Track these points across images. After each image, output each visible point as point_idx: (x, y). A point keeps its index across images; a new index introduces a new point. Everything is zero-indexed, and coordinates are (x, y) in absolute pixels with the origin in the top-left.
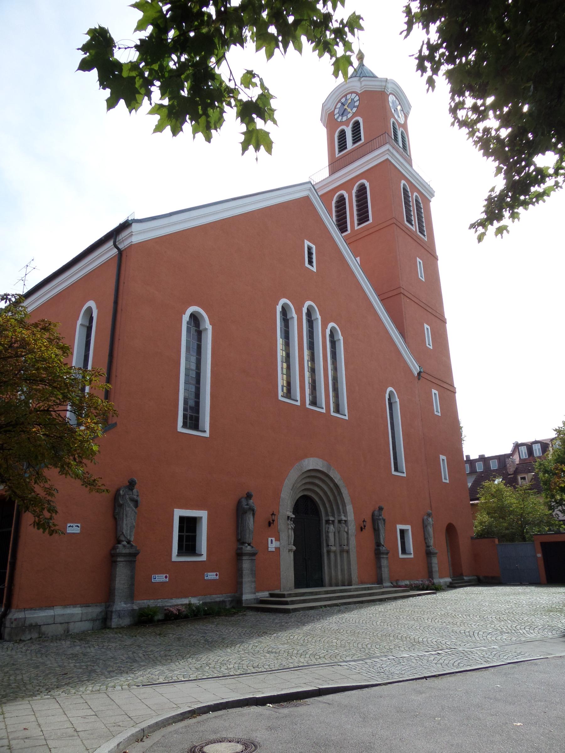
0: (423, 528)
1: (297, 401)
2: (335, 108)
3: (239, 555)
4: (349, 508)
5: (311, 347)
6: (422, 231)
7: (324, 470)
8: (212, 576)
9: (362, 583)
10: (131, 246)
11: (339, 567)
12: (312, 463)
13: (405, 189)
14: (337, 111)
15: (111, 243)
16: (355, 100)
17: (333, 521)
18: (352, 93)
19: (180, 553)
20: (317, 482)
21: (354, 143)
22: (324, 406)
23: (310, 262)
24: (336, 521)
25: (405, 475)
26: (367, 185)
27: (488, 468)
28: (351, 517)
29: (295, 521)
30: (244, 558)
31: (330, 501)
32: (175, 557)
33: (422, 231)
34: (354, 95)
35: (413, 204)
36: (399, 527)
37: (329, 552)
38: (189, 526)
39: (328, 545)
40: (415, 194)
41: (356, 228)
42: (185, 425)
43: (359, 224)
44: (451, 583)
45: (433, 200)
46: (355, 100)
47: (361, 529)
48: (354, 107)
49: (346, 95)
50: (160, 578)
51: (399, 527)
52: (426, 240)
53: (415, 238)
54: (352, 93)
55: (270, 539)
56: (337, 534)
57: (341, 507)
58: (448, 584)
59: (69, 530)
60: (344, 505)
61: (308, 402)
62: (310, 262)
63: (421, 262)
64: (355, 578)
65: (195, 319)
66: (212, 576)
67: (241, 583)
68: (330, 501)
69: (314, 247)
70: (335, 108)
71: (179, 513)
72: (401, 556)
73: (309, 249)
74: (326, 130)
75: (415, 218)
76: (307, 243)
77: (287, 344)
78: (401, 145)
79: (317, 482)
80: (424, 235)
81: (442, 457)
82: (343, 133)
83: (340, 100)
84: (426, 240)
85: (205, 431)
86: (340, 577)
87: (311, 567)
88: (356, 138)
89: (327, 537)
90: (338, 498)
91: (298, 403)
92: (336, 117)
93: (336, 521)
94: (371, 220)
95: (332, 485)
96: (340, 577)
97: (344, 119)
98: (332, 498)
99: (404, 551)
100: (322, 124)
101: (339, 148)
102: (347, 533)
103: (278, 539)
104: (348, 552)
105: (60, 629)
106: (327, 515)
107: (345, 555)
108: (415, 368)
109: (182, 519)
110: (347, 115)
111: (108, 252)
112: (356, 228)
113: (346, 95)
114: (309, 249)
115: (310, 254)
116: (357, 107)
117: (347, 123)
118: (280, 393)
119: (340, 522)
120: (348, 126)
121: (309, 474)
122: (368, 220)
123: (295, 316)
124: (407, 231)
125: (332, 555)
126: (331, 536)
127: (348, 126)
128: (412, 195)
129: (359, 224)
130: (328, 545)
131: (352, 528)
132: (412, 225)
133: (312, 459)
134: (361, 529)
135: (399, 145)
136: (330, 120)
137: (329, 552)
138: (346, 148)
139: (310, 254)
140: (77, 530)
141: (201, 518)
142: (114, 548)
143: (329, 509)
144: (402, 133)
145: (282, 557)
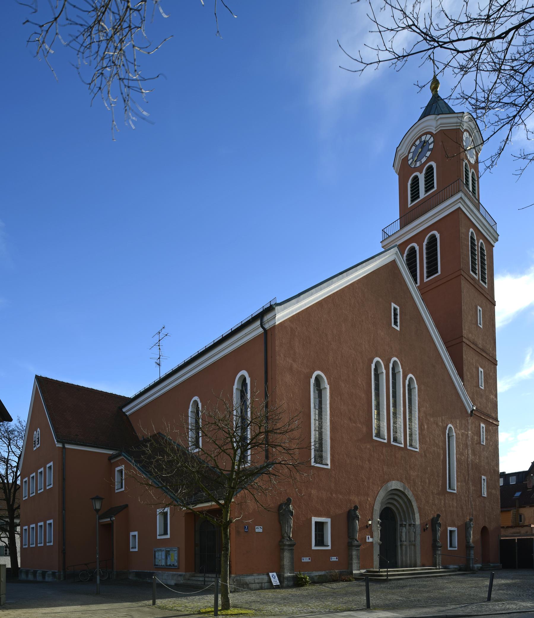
0: (465, 529)
1: (385, 439)
2: (409, 153)
3: (350, 546)
4: (417, 516)
5: (394, 396)
6: (483, 279)
7: (401, 489)
8: (334, 559)
9: (424, 566)
10: (274, 327)
11: (408, 555)
12: (395, 485)
13: (472, 238)
14: (411, 155)
15: (258, 323)
16: (430, 142)
17: (405, 525)
18: (426, 134)
19: (316, 545)
20: (396, 497)
21: (426, 191)
22: (403, 443)
23: (396, 323)
24: (407, 525)
25: (455, 492)
26: (438, 236)
27: (503, 475)
28: (418, 522)
29: (381, 525)
30: (353, 548)
31: (404, 511)
32: (314, 548)
33: (483, 279)
34: (429, 136)
35: (478, 252)
36: (449, 528)
37: (401, 545)
38: (320, 526)
39: (401, 541)
40: (481, 241)
41: (426, 280)
42: (315, 462)
43: (428, 277)
44: (481, 568)
45: (496, 245)
46: (430, 142)
47: (424, 530)
48: (429, 150)
49: (420, 137)
50: (306, 560)
51: (449, 528)
52: (486, 287)
53: (477, 286)
54: (426, 134)
55: (367, 537)
56: (407, 533)
57: (411, 515)
58: (479, 568)
59: (257, 530)
60: (414, 514)
61: (392, 440)
62: (396, 323)
63: (481, 309)
64: (419, 562)
65: (318, 380)
66: (334, 559)
67: (352, 564)
68: (404, 511)
69: (398, 308)
70: (409, 153)
71: (314, 519)
72: (449, 549)
73: (395, 309)
74: (397, 177)
75: (478, 267)
76: (393, 305)
77: (377, 395)
78: (471, 189)
79: (396, 497)
80: (485, 283)
81: (483, 477)
82: (416, 180)
83: (414, 143)
84: (486, 287)
85: (327, 465)
86: (408, 562)
87: (389, 555)
88: (429, 186)
89: (401, 535)
90: (410, 509)
91: (386, 441)
92: (410, 162)
93: (407, 525)
94: (439, 273)
95: (406, 500)
96: (408, 562)
97: (418, 164)
98: (405, 509)
99: (451, 546)
100: (394, 171)
101: (412, 198)
102: (415, 533)
103: (372, 537)
104: (415, 545)
105: (258, 586)
106: (401, 520)
107: (413, 547)
108: (469, 406)
109: (316, 523)
110: (420, 160)
111: (256, 330)
112: (426, 280)
113: (420, 137)
114: (395, 309)
115: (396, 315)
116: (431, 150)
117: (420, 169)
118: (374, 435)
119: (410, 525)
120: (421, 172)
121: (391, 493)
122: (437, 272)
123: (384, 371)
124: (480, 290)
125: (404, 547)
126: (404, 535)
127: (421, 172)
128: (478, 242)
129: (428, 277)
130: (401, 541)
131: (418, 530)
132: (476, 274)
133: (394, 482)
134: (424, 530)
135: (469, 190)
136: (404, 169)
137: (401, 545)
138: (418, 197)
139: (396, 315)
140: (260, 530)
141: (327, 522)
142: (281, 541)
143: (403, 517)
144: (473, 173)
145: (374, 548)
